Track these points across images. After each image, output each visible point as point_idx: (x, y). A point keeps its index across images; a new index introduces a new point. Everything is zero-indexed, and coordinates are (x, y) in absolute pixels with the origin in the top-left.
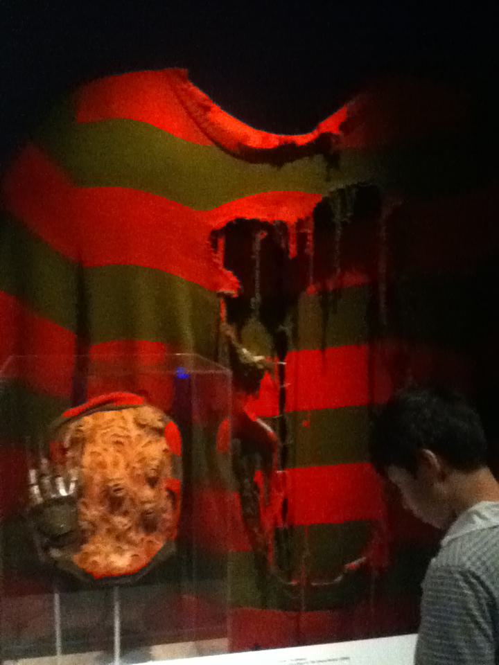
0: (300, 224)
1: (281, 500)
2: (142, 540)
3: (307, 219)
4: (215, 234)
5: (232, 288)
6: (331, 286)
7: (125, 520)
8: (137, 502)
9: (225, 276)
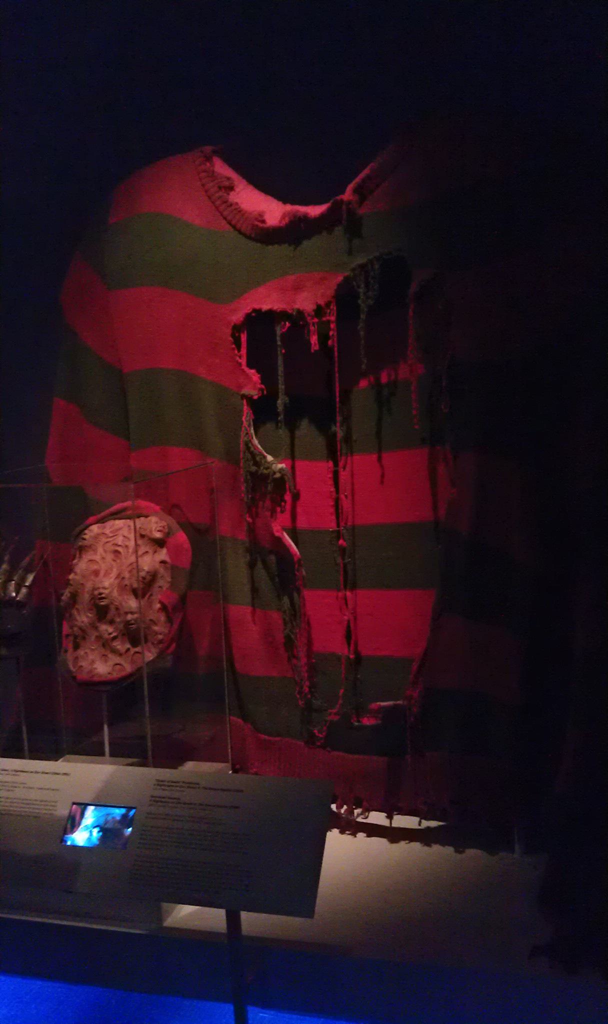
0: (319, 311)
1: (346, 623)
2: (128, 650)
3: (328, 305)
4: (236, 330)
5: (254, 389)
6: (384, 379)
7: (110, 630)
8: (122, 612)
9: (247, 375)
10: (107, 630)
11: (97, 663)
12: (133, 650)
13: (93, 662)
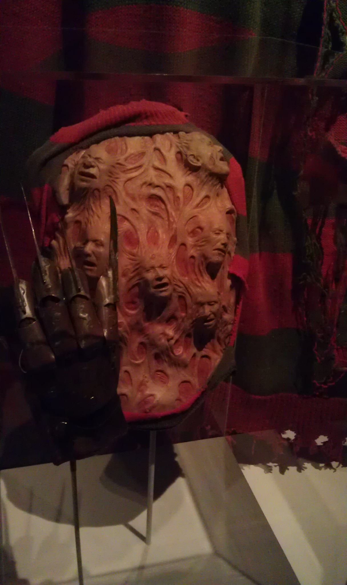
2: (194, 355)
10: (164, 334)
11: (150, 383)
12: (199, 354)
13: (142, 385)
